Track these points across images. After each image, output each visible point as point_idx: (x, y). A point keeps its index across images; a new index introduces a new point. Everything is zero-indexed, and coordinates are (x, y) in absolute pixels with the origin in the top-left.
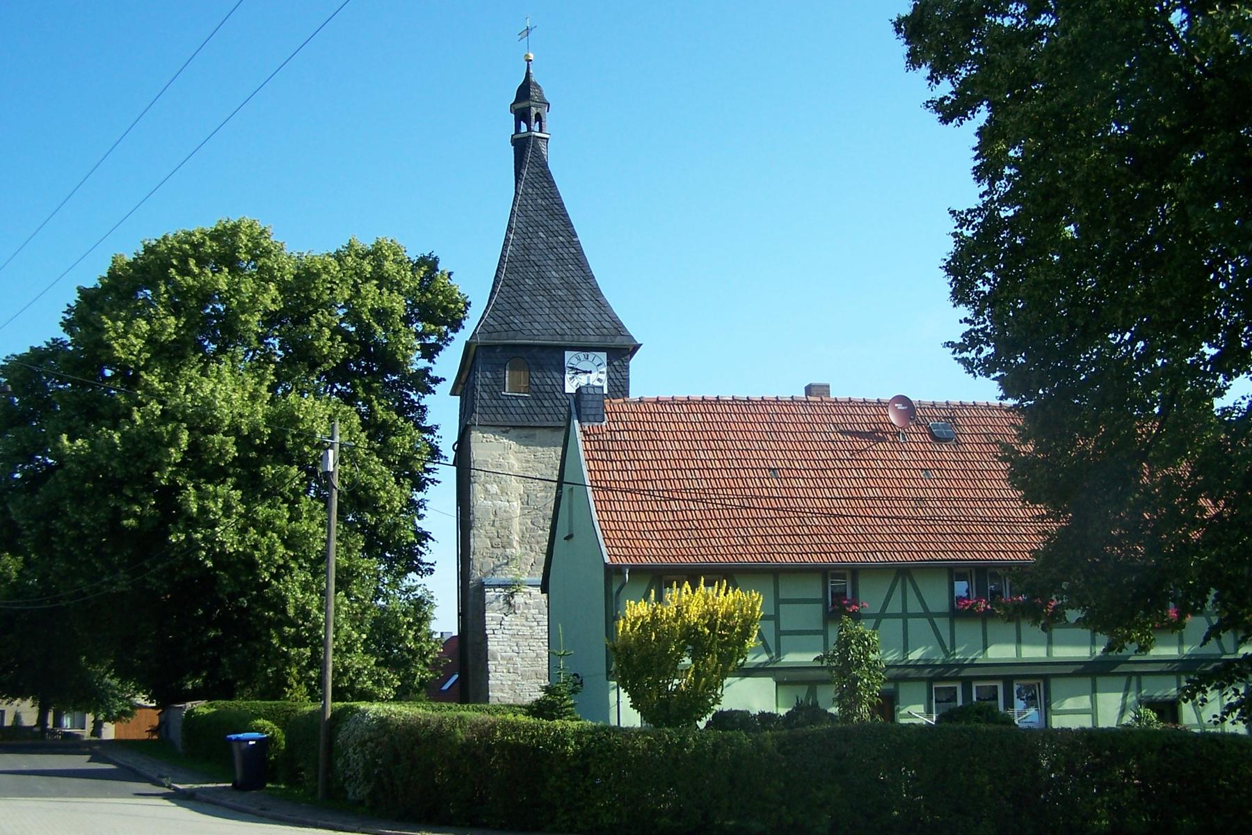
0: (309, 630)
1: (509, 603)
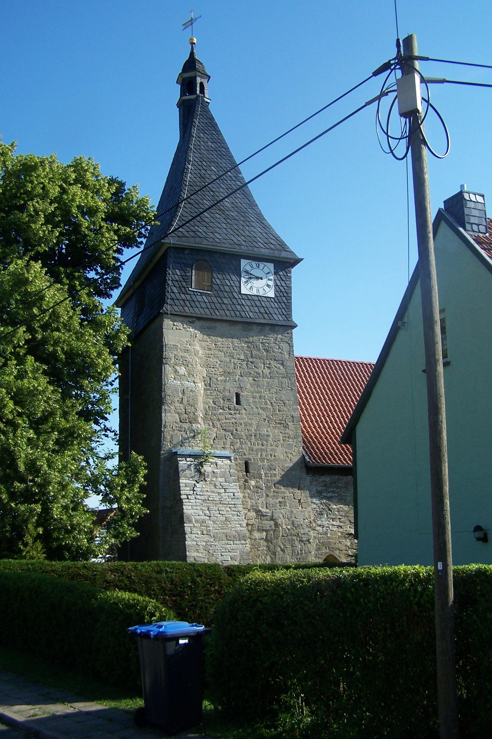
0: (39, 486)
1: (199, 471)
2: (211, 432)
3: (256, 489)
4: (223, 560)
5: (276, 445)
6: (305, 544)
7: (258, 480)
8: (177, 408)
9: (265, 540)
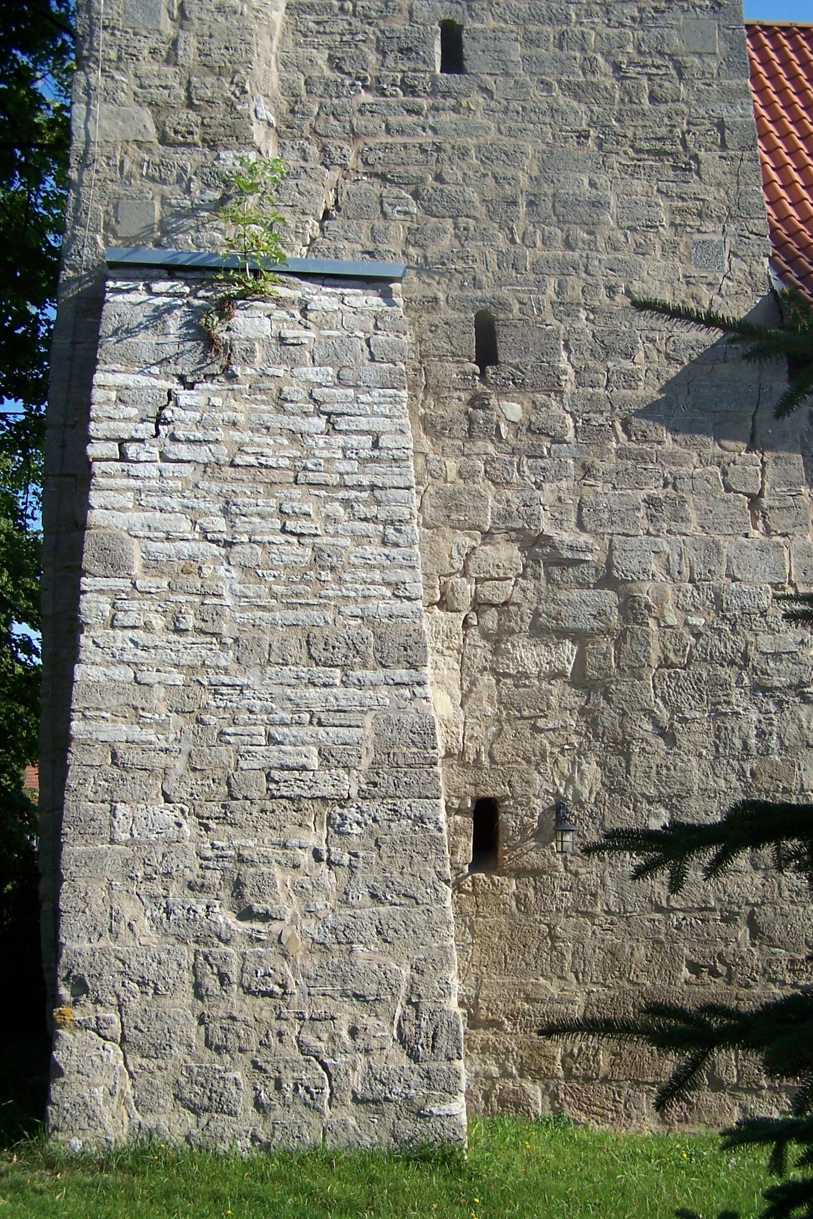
2: (311, 186)
3: (526, 440)
4: (274, 762)
5: (639, 245)
6: (780, 704)
7: (540, 397)
8: (147, 82)
9: (572, 684)
